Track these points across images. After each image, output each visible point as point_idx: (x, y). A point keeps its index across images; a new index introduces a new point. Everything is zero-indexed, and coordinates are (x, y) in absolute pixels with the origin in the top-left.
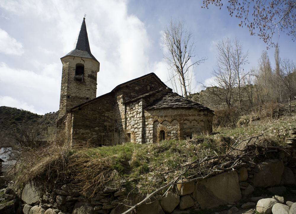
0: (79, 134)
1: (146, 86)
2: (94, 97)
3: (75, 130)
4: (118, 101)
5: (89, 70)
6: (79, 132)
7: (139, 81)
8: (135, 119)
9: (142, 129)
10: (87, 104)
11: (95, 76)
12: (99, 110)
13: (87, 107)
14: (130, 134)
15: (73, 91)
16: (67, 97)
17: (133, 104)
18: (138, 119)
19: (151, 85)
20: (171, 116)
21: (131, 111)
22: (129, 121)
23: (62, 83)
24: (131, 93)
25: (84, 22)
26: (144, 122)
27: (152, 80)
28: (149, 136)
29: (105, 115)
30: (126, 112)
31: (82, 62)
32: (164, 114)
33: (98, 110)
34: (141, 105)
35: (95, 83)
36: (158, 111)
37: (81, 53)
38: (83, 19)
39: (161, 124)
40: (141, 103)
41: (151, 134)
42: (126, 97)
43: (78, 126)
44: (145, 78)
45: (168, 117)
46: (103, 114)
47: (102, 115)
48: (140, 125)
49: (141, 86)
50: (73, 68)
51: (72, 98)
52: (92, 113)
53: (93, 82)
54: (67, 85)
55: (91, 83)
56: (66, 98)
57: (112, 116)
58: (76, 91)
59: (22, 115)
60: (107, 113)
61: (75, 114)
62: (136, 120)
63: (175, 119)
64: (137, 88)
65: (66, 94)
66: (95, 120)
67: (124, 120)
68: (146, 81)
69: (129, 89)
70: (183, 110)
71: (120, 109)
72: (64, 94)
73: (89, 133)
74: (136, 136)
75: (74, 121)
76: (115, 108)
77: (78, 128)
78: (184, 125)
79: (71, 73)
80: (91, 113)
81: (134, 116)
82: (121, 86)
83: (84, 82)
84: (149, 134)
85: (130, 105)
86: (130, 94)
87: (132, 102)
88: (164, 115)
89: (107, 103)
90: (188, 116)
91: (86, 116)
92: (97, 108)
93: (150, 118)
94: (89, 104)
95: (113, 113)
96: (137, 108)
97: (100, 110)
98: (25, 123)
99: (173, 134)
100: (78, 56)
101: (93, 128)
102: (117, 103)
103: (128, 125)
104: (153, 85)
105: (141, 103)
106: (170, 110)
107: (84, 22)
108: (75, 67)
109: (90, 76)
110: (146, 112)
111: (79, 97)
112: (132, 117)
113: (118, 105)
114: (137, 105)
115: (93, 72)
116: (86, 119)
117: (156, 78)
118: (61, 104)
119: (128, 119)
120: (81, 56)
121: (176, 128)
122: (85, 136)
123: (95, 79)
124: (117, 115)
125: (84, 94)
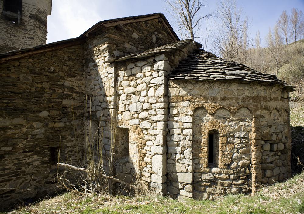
2: (36, 43)
4: (96, 57)
5: (33, 7)
7: (139, 22)
9: (164, 124)
10: (16, 57)
13: (17, 64)
14: (127, 130)
17: (136, 66)
20: (237, 99)
22: (125, 102)
24: (124, 42)
26: (168, 109)
29: (66, 84)
30: (116, 81)
32: (219, 94)
33: (48, 74)
34: (162, 68)
35: (43, 30)
36: (207, 86)
39: (212, 115)
41: (188, 138)
42: (115, 50)
45: (228, 100)
46: (59, 83)
47: (57, 85)
48: (157, 114)
49: (143, 33)
55: (36, 28)
57: (79, 87)
60: (69, 79)
62: (143, 102)
63: (244, 107)
64: (135, 35)
66: (40, 94)
67: (112, 98)
68: (150, 26)
69: (121, 35)
70: (262, 89)
71: (100, 73)
73: (22, 125)
74: (147, 137)
78: (261, 120)
80: (29, 79)
81: (140, 92)
82: (107, 25)
84: (182, 137)
85: (129, 67)
86: (122, 45)
87: (135, 61)
88: (219, 96)
89: (70, 59)
90: (268, 101)
92: (47, 68)
93: (183, 100)
94: (22, 58)
95: (83, 81)
96: (148, 74)
97: (53, 72)
99: (238, 138)
101: (33, 112)
102: (94, 61)
104: (160, 36)
105: (160, 65)
106: (234, 86)
110: (175, 85)
112: (134, 93)
113: (96, 65)
114: (147, 69)
116: (16, 93)
117: (165, 24)
119: (123, 97)
121: (245, 126)
122: (9, 132)
124: (92, 85)
125: (22, 44)
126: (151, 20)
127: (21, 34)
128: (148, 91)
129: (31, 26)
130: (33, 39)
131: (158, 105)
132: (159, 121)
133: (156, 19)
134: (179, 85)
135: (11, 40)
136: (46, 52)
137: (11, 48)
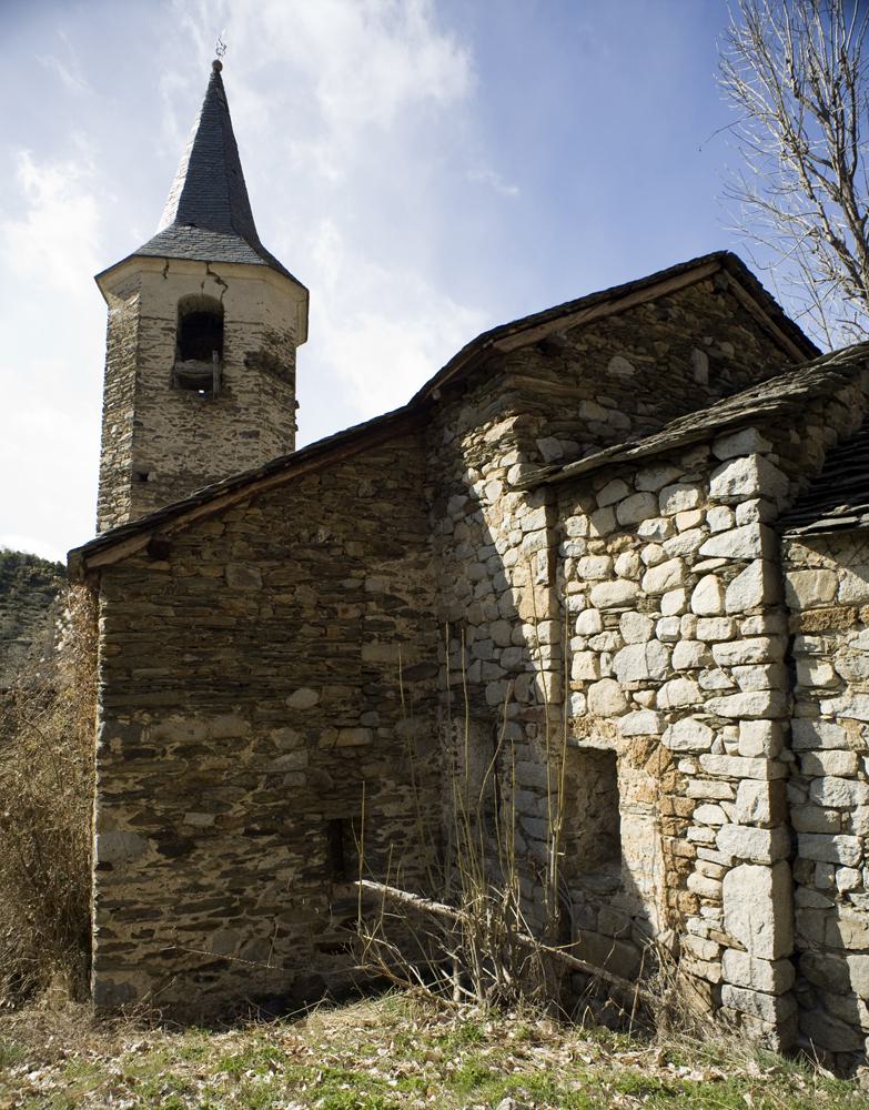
0: (152, 753)
1: (684, 350)
3: (123, 721)
4: (471, 472)
5: (254, 328)
6: (160, 738)
7: (633, 307)
8: (667, 628)
10: (214, 507)
11: (283, 359)
12: (318, 547)
13: (216, 529)
15: (165, 444)
16: (132, 480)
17: (634, 490)
18: (718, 629)
19: (713, 345)
21: (619, 551)
22: (596, 644)
23: (106, 405)
25: (216, 86)
26: (787, 665)
27: (718, 308)
28: (854, 807)
29: (371, 586)
30: (556, 557)
31: (213, 290)
33: (309, 553)
34: (749, 487)
35: (286, 399)
37: (205, 241)
38: (211, 70)
40: (740, 474)
43: (148, 685)
44: (669, 294)
46: (349, 584)
47: (342, 590)
48: (736, 689)
49: (652, 351)
50: (163, 324)
51: (159, 485)
52: (258, 575)
53: (275, 391)
54: (131, 414)
55: (264, 398)
56: (129, 486)
57: (415, 593)
58: (181, 443)
59: (6, 571)
60: (380, 566)
61: (121, 592)
62: (676, 640)
64: (621, 366)
65: (128, 461)
67: (544, 630)
69: (563, 373)
72: (117, 466)
74: (696, 788)
75: (115, 649)
76: (445, 525)
77: (149, 709)
79: (153, 352)
81: (658, 596)
83: (226, 392)
85: (603, 499)
86: (571, 414)
87: (628, 471)
89: (380, 493)
91: (215, 605)
92: (305, 533)
94: (231, 507)
95: (431, 570)
97: (326, 547)
98: (16, 599)
100: (187, 255)
101: (270, 693)
102: (466, 489)
103: (581, 667)
104: (728, 349)
105: (740, 474)
107: (216, 86)
108: (175, 316)
109: (259, 362)
110: (815, 558)
111: (202, 476)
112: (631, 604)
113: (474, 505)
115: (271, 338)
116: (216, 629)
117: (743, 293)
118: (104, 518)
119: (587, 622)
120: (206, 256)
122: (206, 763)
123: (287, 376)
125: (226, 460)
126: (682, 289)
127: (222, 425)
128: (690, 592)
129: (248, 392)
130: (256, 434)
131: (741, 648)
132: (747, 718)
133: (702, 280)
134: (834, 555)
135: (195, 452)
136: (301, 478)
137: (194, 476)
